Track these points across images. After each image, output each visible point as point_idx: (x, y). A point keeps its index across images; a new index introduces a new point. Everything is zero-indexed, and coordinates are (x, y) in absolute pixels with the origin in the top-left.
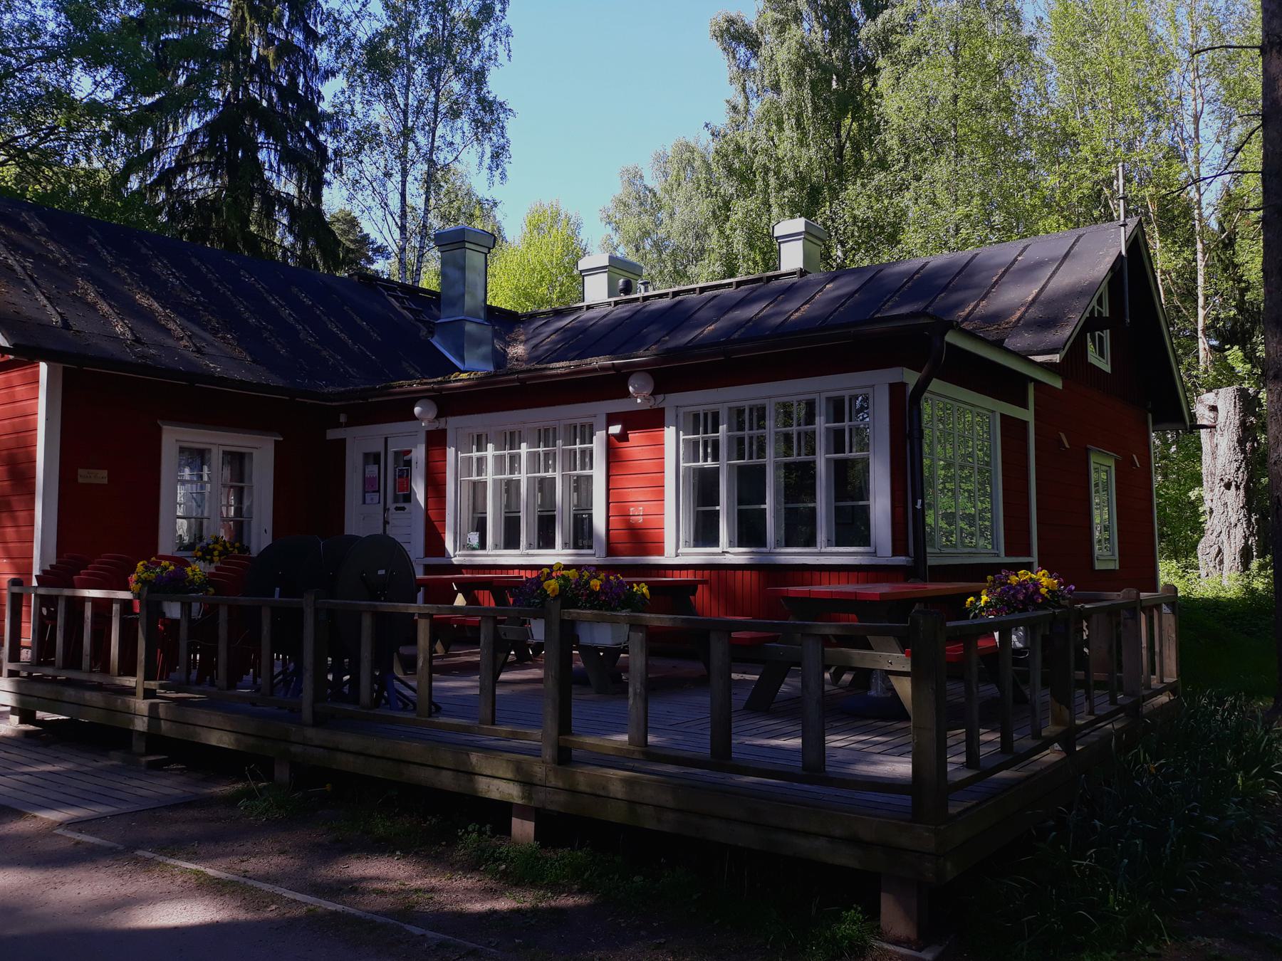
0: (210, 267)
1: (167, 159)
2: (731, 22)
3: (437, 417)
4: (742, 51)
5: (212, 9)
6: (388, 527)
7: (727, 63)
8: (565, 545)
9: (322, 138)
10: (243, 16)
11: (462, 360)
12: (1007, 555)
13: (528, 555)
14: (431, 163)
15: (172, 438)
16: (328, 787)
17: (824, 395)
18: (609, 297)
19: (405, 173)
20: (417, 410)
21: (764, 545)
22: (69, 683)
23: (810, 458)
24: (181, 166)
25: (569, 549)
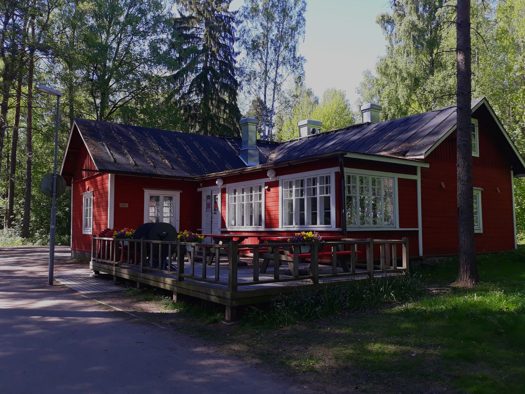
0: (167, 138)
1: (185, 90)
2: (383, 17)
3: (223, 184)
4: (389, 27)
5: (198, 36)
6: (212, 219)
7: (382, 32)
8: (321, 224)
9: (235, 77)
10: (207, 37)
11: (248, 163)
12: (400, 227)
13: (246, 228)
14: (275, 83)
15: (148, 193)
16: (145, 289)
17: (319, 176)
18: (308, 135)
19: (266, 87)
20: (217, 182)
21: (304, 224)
22: (101, 262)
23: (260, 201)
24: (190, 92)
25: (298, 225)
